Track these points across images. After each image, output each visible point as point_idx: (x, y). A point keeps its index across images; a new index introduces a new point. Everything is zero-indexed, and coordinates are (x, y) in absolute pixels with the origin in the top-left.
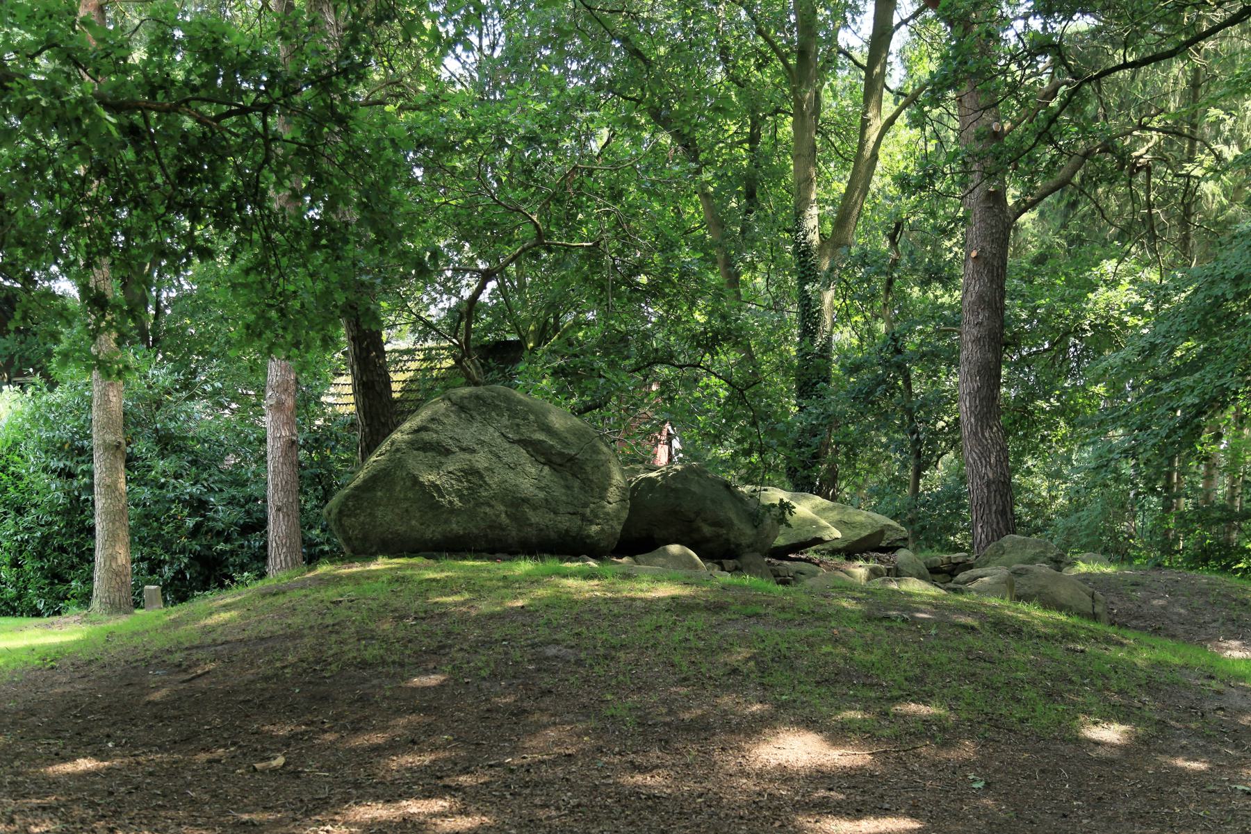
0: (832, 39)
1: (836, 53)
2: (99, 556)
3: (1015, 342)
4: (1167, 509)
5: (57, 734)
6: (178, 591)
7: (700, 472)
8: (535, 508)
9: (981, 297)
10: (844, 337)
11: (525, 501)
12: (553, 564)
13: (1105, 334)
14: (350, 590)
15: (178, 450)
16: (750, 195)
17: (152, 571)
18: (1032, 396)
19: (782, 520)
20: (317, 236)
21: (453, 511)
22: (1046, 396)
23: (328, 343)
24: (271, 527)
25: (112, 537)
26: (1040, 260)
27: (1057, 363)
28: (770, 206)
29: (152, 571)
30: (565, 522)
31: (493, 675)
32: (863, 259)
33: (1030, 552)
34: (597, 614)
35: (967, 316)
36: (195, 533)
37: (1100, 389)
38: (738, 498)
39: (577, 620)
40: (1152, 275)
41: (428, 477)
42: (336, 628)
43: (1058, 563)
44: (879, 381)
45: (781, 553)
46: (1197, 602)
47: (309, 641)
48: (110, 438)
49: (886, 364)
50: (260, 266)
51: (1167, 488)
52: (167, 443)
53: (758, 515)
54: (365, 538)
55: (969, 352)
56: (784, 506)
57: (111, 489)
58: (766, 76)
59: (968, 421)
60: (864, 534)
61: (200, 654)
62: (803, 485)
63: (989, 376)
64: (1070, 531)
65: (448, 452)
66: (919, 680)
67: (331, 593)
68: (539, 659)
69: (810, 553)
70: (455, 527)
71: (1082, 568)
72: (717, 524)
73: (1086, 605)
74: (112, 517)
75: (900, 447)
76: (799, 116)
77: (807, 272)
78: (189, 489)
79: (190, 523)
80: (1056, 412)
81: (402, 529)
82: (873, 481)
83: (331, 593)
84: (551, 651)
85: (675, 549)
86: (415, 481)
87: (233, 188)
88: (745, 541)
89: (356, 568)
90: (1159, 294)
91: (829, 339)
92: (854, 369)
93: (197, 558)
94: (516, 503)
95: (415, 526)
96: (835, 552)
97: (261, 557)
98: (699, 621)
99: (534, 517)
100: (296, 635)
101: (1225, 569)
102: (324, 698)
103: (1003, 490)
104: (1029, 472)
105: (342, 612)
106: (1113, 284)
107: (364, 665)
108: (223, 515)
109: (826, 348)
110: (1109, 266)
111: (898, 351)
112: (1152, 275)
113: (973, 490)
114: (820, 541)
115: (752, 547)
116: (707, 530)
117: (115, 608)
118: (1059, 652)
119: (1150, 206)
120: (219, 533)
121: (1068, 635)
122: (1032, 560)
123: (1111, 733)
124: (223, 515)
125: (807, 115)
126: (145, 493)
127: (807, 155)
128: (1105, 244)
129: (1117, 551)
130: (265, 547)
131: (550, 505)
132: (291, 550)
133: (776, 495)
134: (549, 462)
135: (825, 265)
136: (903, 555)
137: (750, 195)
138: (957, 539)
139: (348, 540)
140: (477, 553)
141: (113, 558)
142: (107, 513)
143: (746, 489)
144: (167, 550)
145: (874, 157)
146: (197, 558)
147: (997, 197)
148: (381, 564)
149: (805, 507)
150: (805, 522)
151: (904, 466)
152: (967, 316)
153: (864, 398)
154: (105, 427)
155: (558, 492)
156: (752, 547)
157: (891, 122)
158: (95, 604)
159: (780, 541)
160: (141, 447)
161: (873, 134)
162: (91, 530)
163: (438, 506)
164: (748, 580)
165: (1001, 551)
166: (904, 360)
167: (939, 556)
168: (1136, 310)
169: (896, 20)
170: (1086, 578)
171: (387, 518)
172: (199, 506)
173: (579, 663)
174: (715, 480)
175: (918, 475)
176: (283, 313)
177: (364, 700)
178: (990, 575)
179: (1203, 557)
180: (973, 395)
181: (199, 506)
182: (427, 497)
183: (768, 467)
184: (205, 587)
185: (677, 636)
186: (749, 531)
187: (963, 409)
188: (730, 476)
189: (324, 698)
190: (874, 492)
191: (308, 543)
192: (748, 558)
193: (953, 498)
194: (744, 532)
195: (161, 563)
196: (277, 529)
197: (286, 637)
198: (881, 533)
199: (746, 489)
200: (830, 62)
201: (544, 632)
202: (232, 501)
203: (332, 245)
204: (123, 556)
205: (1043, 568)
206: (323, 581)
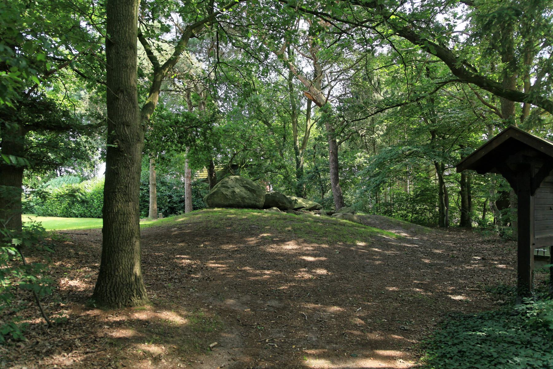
0: (299, 109)
1: (300, 112)
2: (150, 207)
3: (341, 168)
4: (377, 202)
5: (156, 240)
6: (166, 215)
7: (278, 193)
8: (246, 199)
9: (333, 160)
10: (305, 165)
11: (245, 198)
12: (251, 210)
13: (359, 167)
14: (211, 214)
15: (165, 185)
16: (284, 138)
17: (160, 210)
18: (346, 179)
19: (296, 203)
20: (205, 148)
21: (230, 199)
22: (348, 179)
23: (203, 168)
24: (186, 201)
25: (153, 203)
26: (345, 152)
27: (352, 172)
28: (289, 140)
29: (160, 210)
30: (253, 202)
31: (242, 231)
32: (309, 151)
33: (347, 211)
34: (262, 220)
35: (331, 163)
36: (169, 202)
37: (360, 178)
38: (287, 198)
39: (258, 220)
40: (368, 156)
41: (225, 193)
42: (210, 221)
43: (353, 213)
44: (313, 176)
45: (296, 209)
46: (382, 221)
47: (204, 223)
48: (153, 183)
49: (314, 172)
50: (194, 153)
51: (377, 198)
52: (163, 183)
53: (291, 202)
54: (212, 204)
55: (331, 170)
56: (296, 200)
57: (153, 193)
58: (286, 115)
59: (333, 184)
60: (532, 208)
61: (183, 226)
62: (299, 196)
63: (336, 175)
64: (356, 207)
65: (229, 188)
66: (325, 233)
67: (207, 215)
68: (251, 228)
69: (302, 210)
70: (231, 202)
71: (358, 214)
72: (283, 203)
73: (359, 221)
74: (153, 199)
75: (319, 189)
76: (293, 123)
77: (297, 154)
78: (168, 193)
79: (168, 200)
80: (351, 182)
81: (220, 202)
82: (314, 195)
83: (207, 215)
84: (253, 226)
85: (275, 208)
86: (222, 193)
87: (189, 140)
88: (288, 207)
89: (211, 210)
90: (369, 160)
91: (302, 166)
92: (308, 173)
93: (169, 207)
94: (243, 198)
95: (223, 202)
96: (307, 210)
97: (184, 208)
98: (282, 221)
99: (246, 201)
100: (201, 222)
101: (390, 215)
102: (209, 234)
103: (341, 198)
104: (347, 194)
105: (210, 218)
106: (360, 157)
107: (216, 228)
108: (175, 199)
109: (302, 168)
110: (359, 154)
111: (317, 170)
112: (368, 156)
113: (335, 198)
114: (304, 207)
115: (290, 208)
116: (281, 204)
117: (154, 218)
118: (352, 229)
119: (366, 143)
120: (175, 202)
121: (353, 226)
122: (348, 212)
123: (362, 244)
124: (175, 199)
125: (295, 123)
126: (159, 194)
127: (296, 131)
128: (358, 149)
129: (366, 211)
130: (184, 206)
131: (250, 199)
132: (190, 206)
133: (294, 198)
134: (249, 190)
135: (301, 152)
136: (321, 210)
137: (284, 138)
138: (333, 208)
139: (209, 204)
140: (235, 207)
141: (153, 207)
142: (152, 198)
143: (288, 196)
144: (163, 206)
145: (309, 132)
146: (169, 207)
147: (335, 141)
148: (216, 209)
149: (300, 200)
150: (300, 203)
151: (320, 193)
152: (331, 163)
153: (311, 179)
154: (153, 180)
155: (251, 196)
156: (290, 208)
157: (312, 125)
158: (149, 216)
159: (296, 207)
160: (158, 184)
161: (309, 128)
162: (148, 202)
163: (227, 198)
164: (290, 214)
165: (341, 210)
166: (316, 9)
167: (328, 211)
168: (365, 163)
169: (312, 107)
170: (359, 216)
171: (217, 200)
172: (170, 197)
173: (259, 229)
174: (282, 195)
175: (323, 194)
176: (198, 162)
177: (217, 235)
178: (339, 215)
179: (385, 213)
180: (333, 179)
181: (170, 197)
182: (225, 196)
183: (292, 192)
184: (171, 213)
185: (278, 224)
186: (289, 205)
187: (331, 182)
188: (284, 193)
189: (209, 234)
190: (314, 198)
191: (194, 205)
192: (289, 210)
193: (331, 200)
194: (288, 205)
195: (162, 209)
196: (187, 202)
197: (199, 223)
198: (316, 206)
199: (288, 196)
200: (299, 114)
201: (251, 223)
202: (177, 196)
203: (208, 150)
204: (155, 206)
205: (350, 214)
206: (204, 212)
